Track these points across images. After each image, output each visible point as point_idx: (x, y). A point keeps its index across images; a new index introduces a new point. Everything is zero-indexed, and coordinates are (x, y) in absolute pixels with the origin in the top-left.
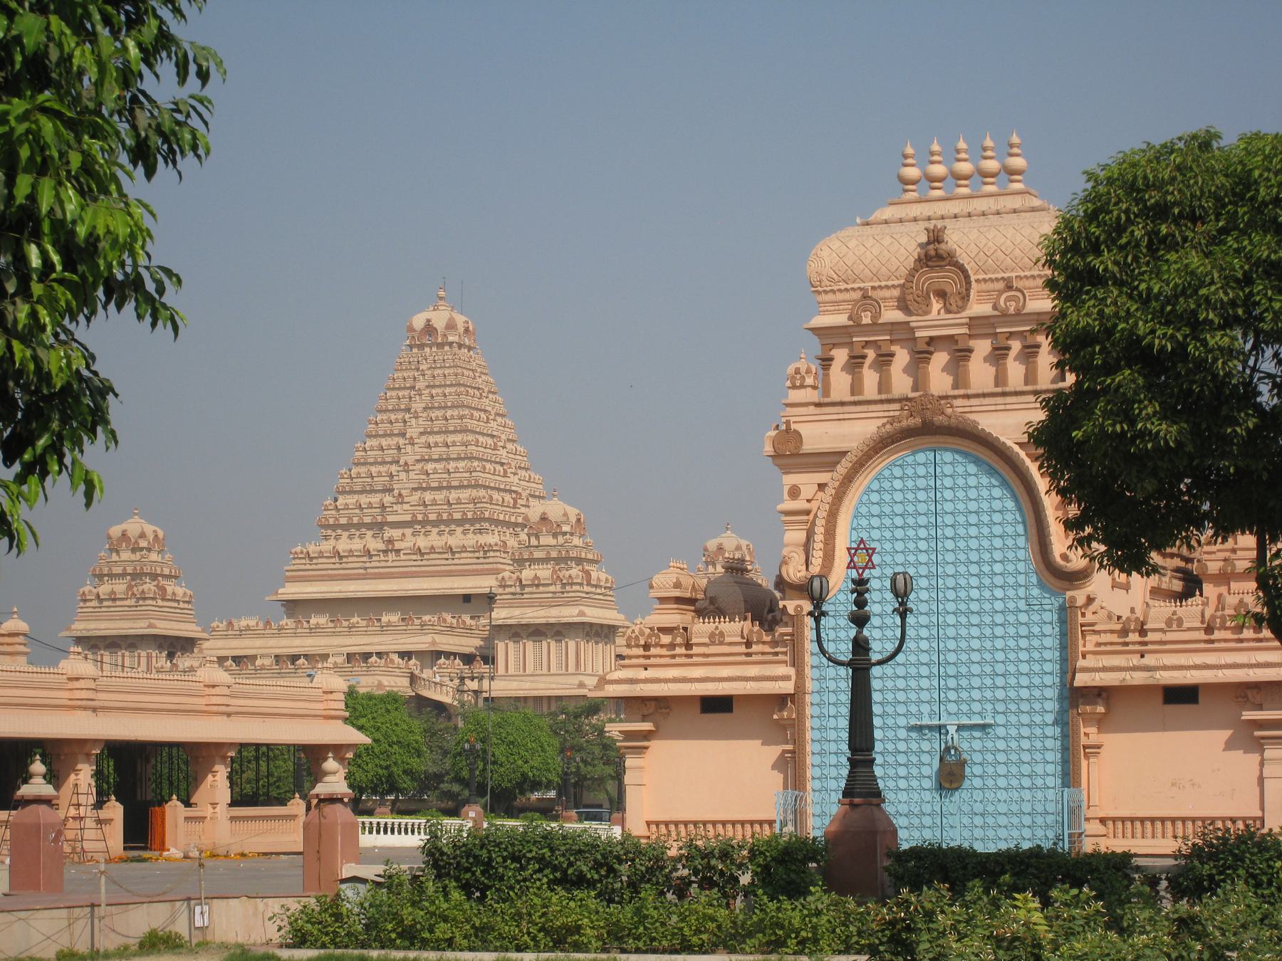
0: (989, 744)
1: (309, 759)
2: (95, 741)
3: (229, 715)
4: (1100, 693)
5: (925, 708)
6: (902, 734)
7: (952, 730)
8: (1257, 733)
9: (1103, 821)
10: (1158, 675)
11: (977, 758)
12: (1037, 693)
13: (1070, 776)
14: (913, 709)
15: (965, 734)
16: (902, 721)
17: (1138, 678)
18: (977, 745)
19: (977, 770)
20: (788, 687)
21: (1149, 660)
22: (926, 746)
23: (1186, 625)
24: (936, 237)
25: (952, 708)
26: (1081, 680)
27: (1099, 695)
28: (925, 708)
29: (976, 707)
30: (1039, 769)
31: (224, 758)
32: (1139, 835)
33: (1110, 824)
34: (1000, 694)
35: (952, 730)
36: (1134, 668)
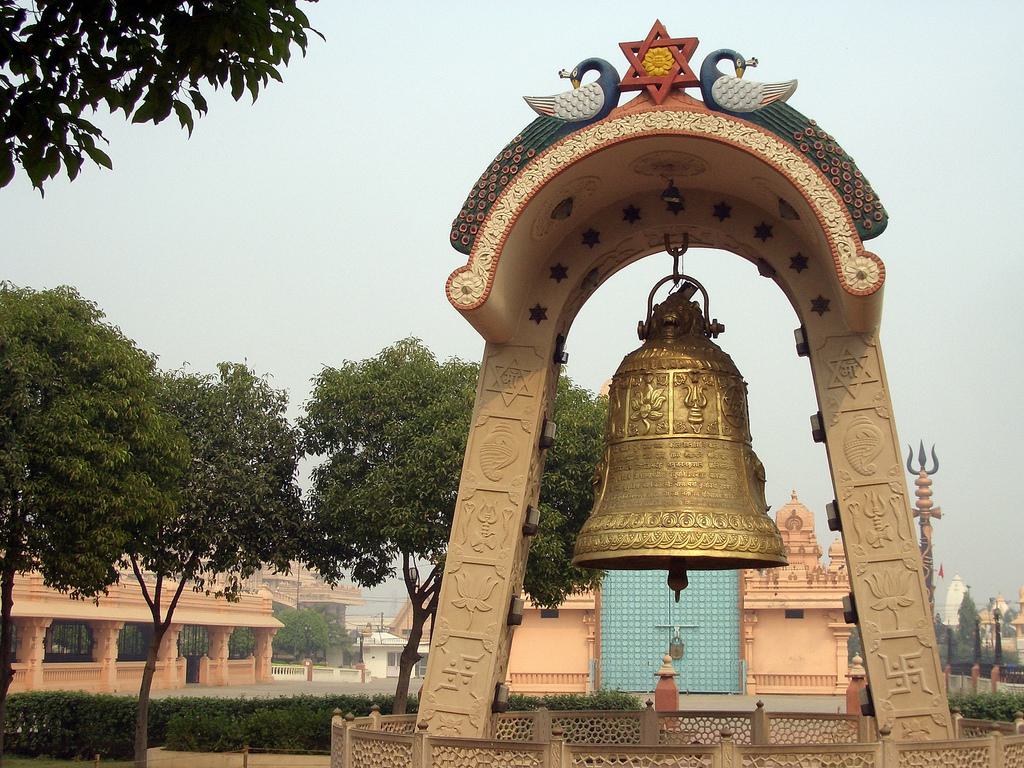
0: (696, 637)
1: (257, 632)
2: (48, 618)
3: (229, 611)
4: (754, 612)
5: (662, 618)
6: (650, 631)
7: (677, 629)
8: (836, 634)
9: (754, 676)
10: (787, 603)
11: (690, 644)
12: (721, 611)
13: (742, 654)
14: (656, 618)
15: (683, 631)
16: (650, 624)
17: (777, 605)
18: (690, 637)
19: (690, 650)
20: (591, 606)
21: (779, 596)
22: (663, 637)
23: (799, 579)
24: (658, 89)
25: (677, 618)
26: (747, 605)
27: (754, 613)
28: (662, 618)
29: (689, 618)
30: (618, 624)
31: (272, 635)
32: (772, 683)
33: (758, 678)
34: (702, 612)
35: (677, 629)
36: (774, 600)
